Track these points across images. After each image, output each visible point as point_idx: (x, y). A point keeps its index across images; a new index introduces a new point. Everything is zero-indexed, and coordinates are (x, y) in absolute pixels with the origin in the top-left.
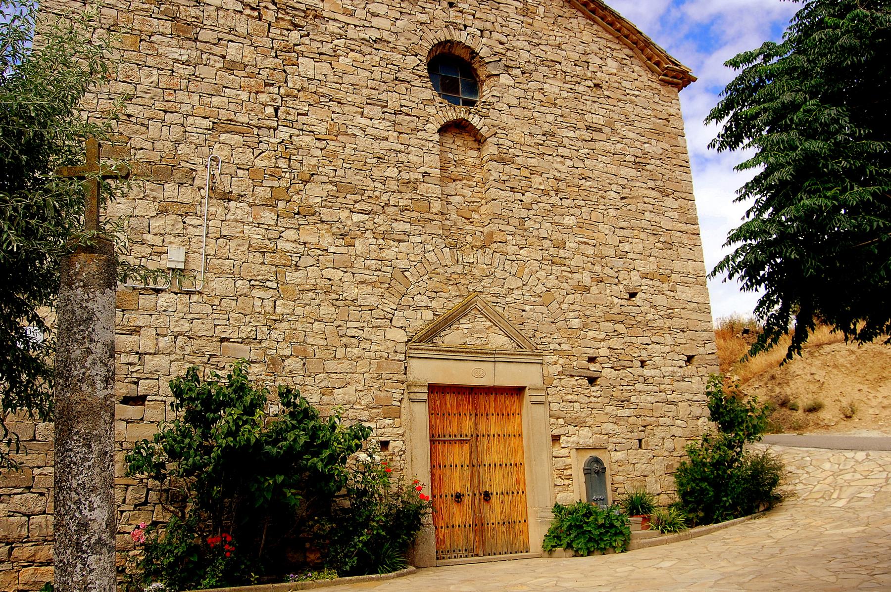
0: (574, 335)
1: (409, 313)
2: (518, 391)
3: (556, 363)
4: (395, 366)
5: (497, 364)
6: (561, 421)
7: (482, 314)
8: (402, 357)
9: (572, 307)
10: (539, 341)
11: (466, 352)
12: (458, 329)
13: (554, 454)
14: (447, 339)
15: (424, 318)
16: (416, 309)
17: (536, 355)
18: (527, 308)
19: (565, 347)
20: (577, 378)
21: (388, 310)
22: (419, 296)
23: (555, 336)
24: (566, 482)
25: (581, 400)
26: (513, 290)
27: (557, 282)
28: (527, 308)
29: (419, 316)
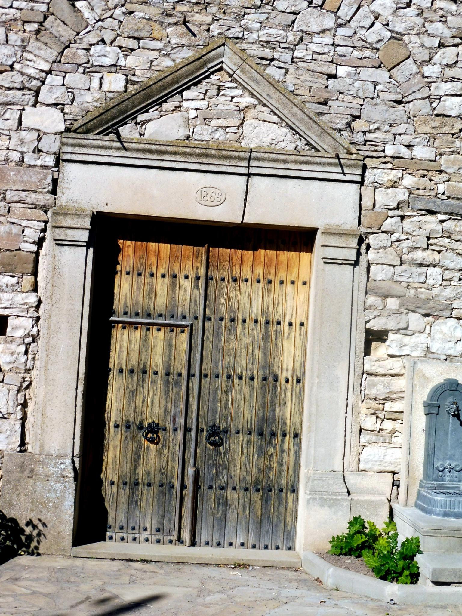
0: (446, 129)
1: (75, 79)
2: (301, 239)
3: (394, 185)
4: (33, 178)
5: (254, 180)
6: (392, 303)
7: (234, 80)
8: (50, 161)
9: (450, 73)
10: (359, 138)
11: (184, 154)
12: (177, 108)
13: (367, 367)
14: (150, 129)
15: (105, 87)
16: (89, 70)
17: (355, 164)
18: (342, 71)
19: (422, 152)
20: (441, 217)
21: (31, 71)
22: (100, 47)
23: (401, 129)
24: (388, 425)
25: (446, 263)
26: (311, 34)
27: (419, 20)
28: (342, 71)
29: (95, 83)
